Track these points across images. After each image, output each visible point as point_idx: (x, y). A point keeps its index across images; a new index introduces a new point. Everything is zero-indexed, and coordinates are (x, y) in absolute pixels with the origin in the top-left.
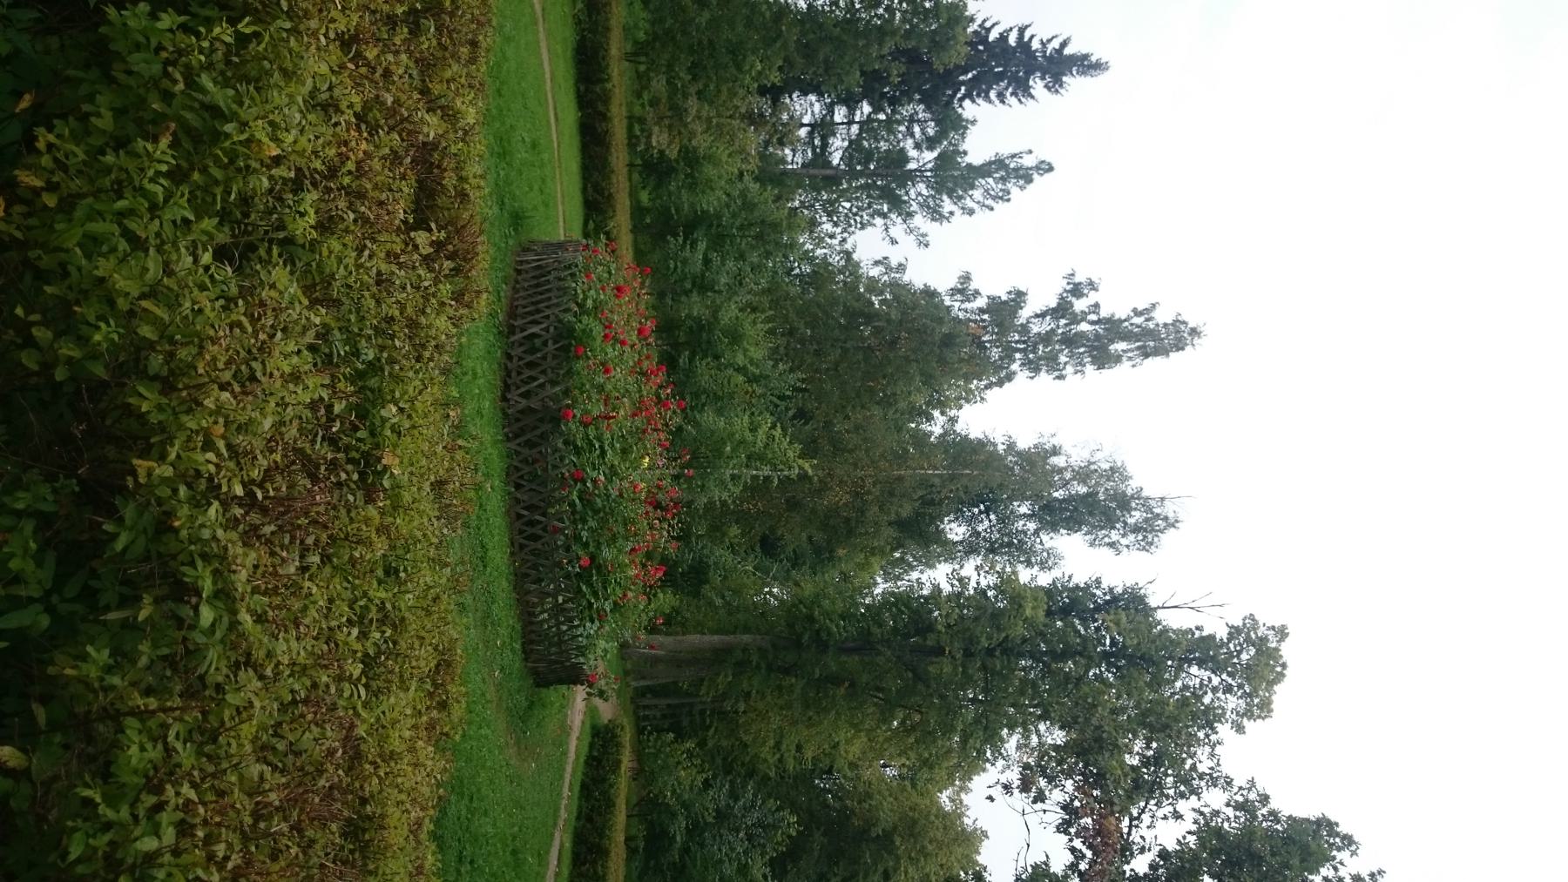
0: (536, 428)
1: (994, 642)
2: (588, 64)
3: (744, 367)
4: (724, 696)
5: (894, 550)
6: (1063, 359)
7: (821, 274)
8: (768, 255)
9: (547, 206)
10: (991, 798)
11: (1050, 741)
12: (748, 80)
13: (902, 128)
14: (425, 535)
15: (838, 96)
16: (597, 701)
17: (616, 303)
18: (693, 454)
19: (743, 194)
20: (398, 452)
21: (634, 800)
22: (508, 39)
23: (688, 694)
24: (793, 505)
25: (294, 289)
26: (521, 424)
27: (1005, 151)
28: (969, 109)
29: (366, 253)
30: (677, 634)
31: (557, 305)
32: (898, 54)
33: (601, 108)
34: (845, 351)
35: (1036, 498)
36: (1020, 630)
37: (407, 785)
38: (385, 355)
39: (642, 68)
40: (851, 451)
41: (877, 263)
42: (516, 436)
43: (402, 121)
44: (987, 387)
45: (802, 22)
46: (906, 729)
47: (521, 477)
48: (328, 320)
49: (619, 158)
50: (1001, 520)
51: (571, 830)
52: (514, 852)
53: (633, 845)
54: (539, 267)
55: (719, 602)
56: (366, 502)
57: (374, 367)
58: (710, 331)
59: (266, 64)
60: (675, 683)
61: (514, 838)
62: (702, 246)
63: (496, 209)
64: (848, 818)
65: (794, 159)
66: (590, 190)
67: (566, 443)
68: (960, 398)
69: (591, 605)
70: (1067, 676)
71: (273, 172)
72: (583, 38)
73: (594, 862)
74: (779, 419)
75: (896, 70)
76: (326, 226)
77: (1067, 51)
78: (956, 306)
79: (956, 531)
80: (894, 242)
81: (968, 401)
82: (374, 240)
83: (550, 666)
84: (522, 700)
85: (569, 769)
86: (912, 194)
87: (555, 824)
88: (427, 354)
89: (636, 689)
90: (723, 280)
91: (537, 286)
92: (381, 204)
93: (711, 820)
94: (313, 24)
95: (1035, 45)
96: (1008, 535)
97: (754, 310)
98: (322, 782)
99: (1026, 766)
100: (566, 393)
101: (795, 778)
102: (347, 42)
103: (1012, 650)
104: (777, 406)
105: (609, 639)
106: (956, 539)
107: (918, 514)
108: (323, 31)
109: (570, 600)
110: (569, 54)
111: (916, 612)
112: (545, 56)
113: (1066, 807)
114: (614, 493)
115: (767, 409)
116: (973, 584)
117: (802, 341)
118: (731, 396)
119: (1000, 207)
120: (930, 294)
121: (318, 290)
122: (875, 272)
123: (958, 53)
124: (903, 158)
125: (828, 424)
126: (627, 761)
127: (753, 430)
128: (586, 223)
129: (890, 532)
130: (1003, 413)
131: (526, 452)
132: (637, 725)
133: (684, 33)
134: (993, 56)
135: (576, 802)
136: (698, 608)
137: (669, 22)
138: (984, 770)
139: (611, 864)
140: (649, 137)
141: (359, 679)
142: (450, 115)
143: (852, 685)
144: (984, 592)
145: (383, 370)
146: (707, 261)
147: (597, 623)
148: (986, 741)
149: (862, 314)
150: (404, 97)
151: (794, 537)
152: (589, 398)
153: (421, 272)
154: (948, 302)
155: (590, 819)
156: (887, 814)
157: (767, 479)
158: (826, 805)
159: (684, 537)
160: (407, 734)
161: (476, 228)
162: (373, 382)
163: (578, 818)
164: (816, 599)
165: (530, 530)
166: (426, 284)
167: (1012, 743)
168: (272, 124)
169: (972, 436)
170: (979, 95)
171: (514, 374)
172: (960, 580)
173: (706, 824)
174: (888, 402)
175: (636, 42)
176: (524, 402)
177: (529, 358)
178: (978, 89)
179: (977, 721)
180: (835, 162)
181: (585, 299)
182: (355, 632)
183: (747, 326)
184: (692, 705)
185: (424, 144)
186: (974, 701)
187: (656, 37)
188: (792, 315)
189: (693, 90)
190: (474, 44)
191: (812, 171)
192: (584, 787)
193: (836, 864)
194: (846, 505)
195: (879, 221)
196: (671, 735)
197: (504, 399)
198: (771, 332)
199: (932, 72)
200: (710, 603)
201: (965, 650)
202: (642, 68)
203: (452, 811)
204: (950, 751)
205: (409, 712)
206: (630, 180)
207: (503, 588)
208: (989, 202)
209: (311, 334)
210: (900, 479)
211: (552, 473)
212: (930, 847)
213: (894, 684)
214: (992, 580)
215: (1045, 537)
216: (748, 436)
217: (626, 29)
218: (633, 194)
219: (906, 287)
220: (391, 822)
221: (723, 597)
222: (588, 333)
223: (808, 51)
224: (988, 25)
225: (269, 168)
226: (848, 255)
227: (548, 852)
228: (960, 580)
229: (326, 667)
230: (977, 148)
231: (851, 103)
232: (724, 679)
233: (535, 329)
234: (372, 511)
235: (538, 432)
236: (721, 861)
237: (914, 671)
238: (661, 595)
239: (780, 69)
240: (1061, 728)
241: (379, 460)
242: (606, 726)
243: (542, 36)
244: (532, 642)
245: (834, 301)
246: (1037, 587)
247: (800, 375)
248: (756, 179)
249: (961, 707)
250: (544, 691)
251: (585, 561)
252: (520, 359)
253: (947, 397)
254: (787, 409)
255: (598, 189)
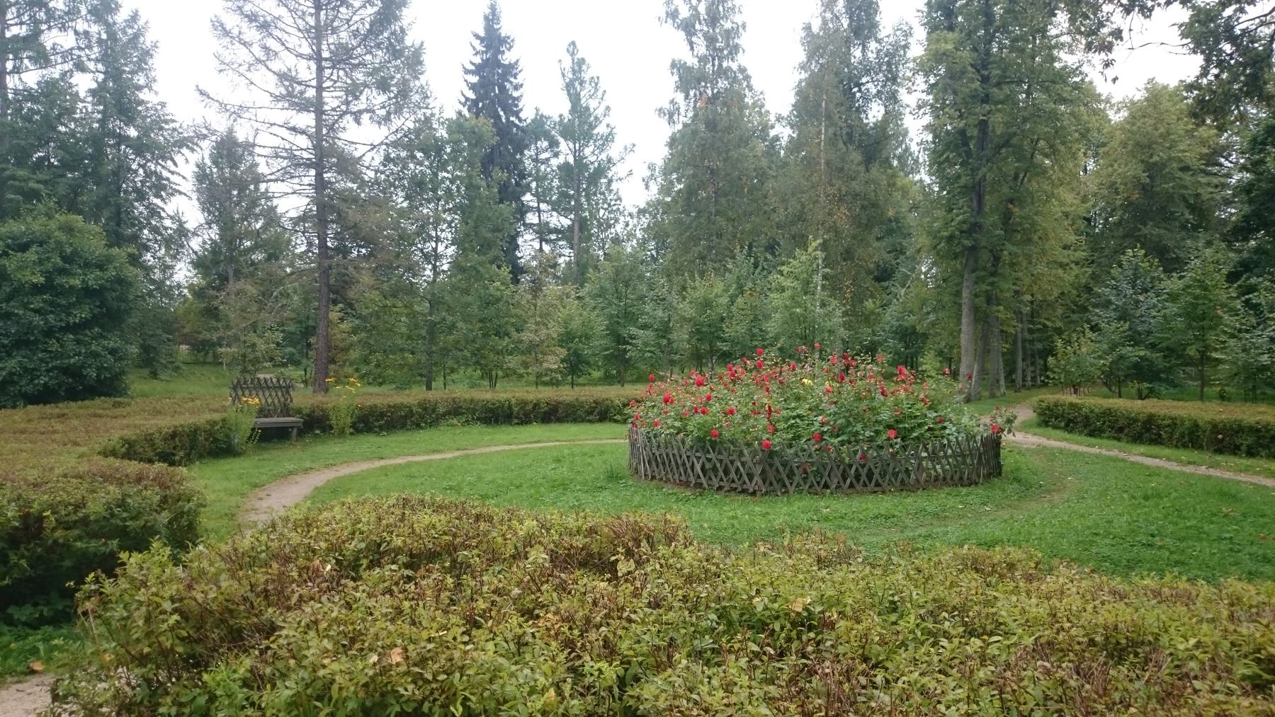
0: (777, 470)
1: (977, 76)
2: (497, 416)
3: (731, 297)
4: (1018, 313)
5: (891, 166)
6: (728, 25)
7: (657, 233)
8: (641, 277)
9: (602, 453)
10: (1115, 80)
11: (1067, 25)
12: (508, 292)
13: (543, 168)
14: (863, 579)
15: (519, 220)
16: (1016, 423)
17: (682, 401)
18: (803, 341)
19: (594, 297)
20: (792, 598)
21: (1105, 390)
22: (480, 478)
23: (1015, 343)
24: (848, 255)
25: (658, 680)
26: (775, 483)
27: (560, 83)
28: (528, 114)
29: (633, 616)
30: (959, 353)
31: (679, 449)
32: (486, 172)
33: (530, 407)
34: (718, 213)
35: (848, 43)
36: (966, 55)
37: (1079, 602)
38: (713, 605)
39: (500, 373)
40: (803, 206)
41: (647, 187)
42: (784, 486)
43: (534, 581)
44: (750, 87)
45: (464, 250)
46: (1053, 152)
47: (818, 483)
48: (685, 651)
49: (566, 394)
50: (867, 72)
51: (1129, 446)
52: (1146, 498)
53: (1145, 392)
54: (649, 462)
55: (932, 317)
56: (833, 628)
57: (723, 615)
58: (701, 324)
59: (486, 694)
60: (1003, 354)
61: (1134, 497)
62: (633, 330)
63: (606, 493)
64: (1131, 204)
65: (566, 256)
66: (591, 417)
67: (790, 446)
68: (760, 113)
69: (930, 429)
70: (1007, 11)
71: (567, 695)
72: (478, 419)
73: (1159, 427)
74: (774, 267)
75: (499, 174)
76: (610, 651)
77: (482, 34)
78: (685, 117)
79: (875, 113)
80: (630, 173)
81: (762, 106)
82: (623, 609)
83: (984, 464)
84: (1012, 488)
85: (1075, 447)
86: (593, 159)
87: (1123, 460)
88: (713, 568)
89: (1007, 387)
90: (660, 313)
91: (664, 464)
92: (595, 603)
93: (1127, 326)
94: (457, 654)
95: (478, 60)
96: (880, 65)
97: (684, 288)
98: (1073, 683)
99: (1089, 47)
100: (748, 445)
101: (1093, 250)
102: (472, 623)
103: (983, 61)
104: (763, 269)
105: (961, 412)
106: (883, 111)
107: (860, 146)
108: (462, 646)
109: (925, 446)
110: (490, 430)
111: (947, 147)
112: (493, 449)
113: (1128, 10)
114: (833, 408)
115: (765, 277)
116: (924, 96)
117: (710, 248)
118: (753, 308)
119: (602, 85)
120: (672, 142)
121: (661, 660)
122: (654, 188)
123: (485, 125)
124: (565, 167)
125: (779, 226)
126: (1069, 398)
127: (782, 290)
128: (616, 421)
129: (875, 171)
130: (774, 80)
131: (797, 479)
132: (1040, 387)
133: (473, 341)
134: (487, 93)
135: (1105, 441)
136: (937, 334)
137: (466, 353)
138: (1091, 83)
139: (1162, 413)
140: (551, 370)
141: (984, 641)
142: (529, 541)
143: (1011, 201)
144: (932, 86)
145: (725, 608)
146: (645, 327)
147: (946, 424)
148: (1065, 82)
149: (689, 199)
150: (515, 579)
151: (876, 252)
152: (754, 427)
153: (649, 569)
154: (679, 127)
155: (1121, 430)
156: (1133, 169)
157: (825, 277)
158: (1119, 224)
159: (871, 349)
160: (1034, 601)
161: (616, 522)
162: (735, 615)
163: (1119, 440)
164: (933, 234)
165: (864, 478)
166: (658, 566)
167: (1067, 59)
168: (530, 694)
169: (793, 101)
170: (517, 106)
171: (734, 485)
172: (920, 107)
173: (1130, 329)
174: (762, 175)
175: (482, 378)
176: (756, 479)
177: (721, 473)
178: (511, 106)
179: (1046, 90)
180: (569, 223)
181: (673, 427)
182: (944, 642)
183: (697, 294)
184: (1024, 341)
185: (552, 561)
186: (1028, 93)
187: (477, 363)
188: (689, 257)
189: (515, 335)
190: (478, 518)
191: (576, 241)
192: (1091, 434)
193: (1172, 213)
194: (849, 210)
195: (614, 186)
196: (1050, 359)
197: (754, 494)
198: (702, 274)
199: (499, 145)
200: (933, 324)
201: (983, 101)
202: (500, 373)
203: (1106, 551)
204: (1072, 114)
205: (1014, 598)
206: (584, 385)
207: (912, 502)
208: (599, 94)
209: (694, 667)
210: (828, 163)
211: (815, 458)
212: (1162, 130)
213: (1012, 165)
214: (920, 79)
215: (881, 35)
216: (788, 293)
217: (473, 386)
218: (594, 383)
219: (667, 162)
220: (1111, 620)
221: (928, 313)
222: (700, 427)
223: (486, 246)
224: (463, 100)
225: (564, 698)
226: (641, 212)
227: (1148, 467)
228: (920, 107)
229: (972, 672)
230: (557, 107)
231: (523, 210)
232: (1001, 312)
233: (698, 467)
234: (842, 624)
235: (781, 469)
236: (1164, 316)
237: (1000, 147)
238: (924, 367)
239: (499, 267)
240: (1055, 15)
241: (798, 614)
242: (1040, 414)
243: (477, 451)
244: (961, 478)
245: (679, 222)
246: (928, 39)
247: (737, 251)
248: (582, 286)
249: (1034, 105)
250: (1004, 469)
251: (891, 433)
252: (721, 480)
253: (759, 124)
254: (766, 260)
255: (590, 413)
